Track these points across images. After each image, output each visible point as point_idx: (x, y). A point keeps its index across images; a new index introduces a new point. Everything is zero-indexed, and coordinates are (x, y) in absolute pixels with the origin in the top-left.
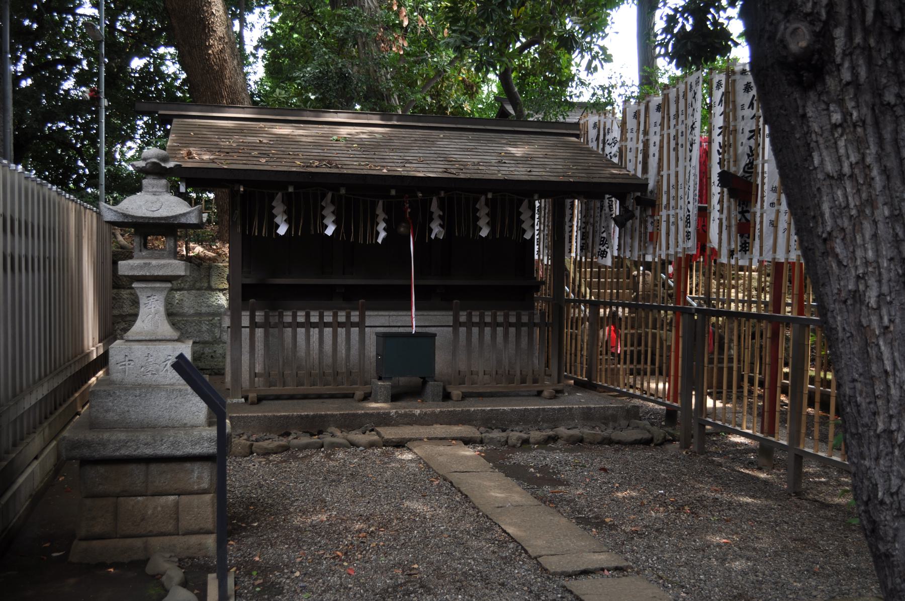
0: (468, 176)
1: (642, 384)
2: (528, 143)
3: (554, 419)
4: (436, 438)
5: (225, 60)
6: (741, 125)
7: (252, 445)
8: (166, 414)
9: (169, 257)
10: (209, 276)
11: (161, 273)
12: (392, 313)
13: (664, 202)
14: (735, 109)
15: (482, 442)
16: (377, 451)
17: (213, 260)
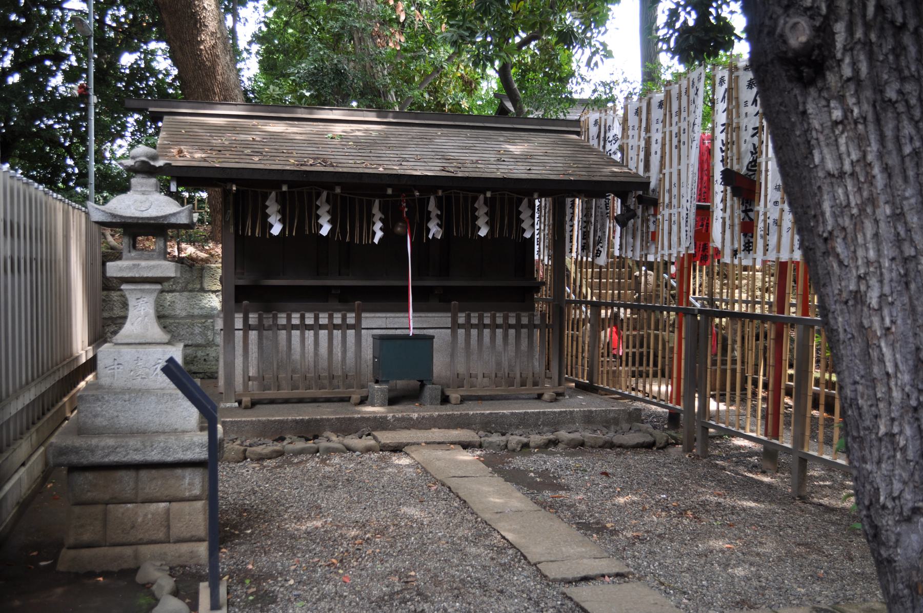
0: (467, 175)
1: (644, 387)
2: (528, 141)
3: (555, 422)
4: (434, 443)
5: (218, 56)
6: (744, 122)
7: (245, 450)
8: (157, 420)
9: (158, 258)
10: (201, 277)
11: (150, 275)
12: (389, 315)
13: (667, 200)
14: (738, 106)
15: (480, 446)
16: (375, 456)
17: (206, 261)
